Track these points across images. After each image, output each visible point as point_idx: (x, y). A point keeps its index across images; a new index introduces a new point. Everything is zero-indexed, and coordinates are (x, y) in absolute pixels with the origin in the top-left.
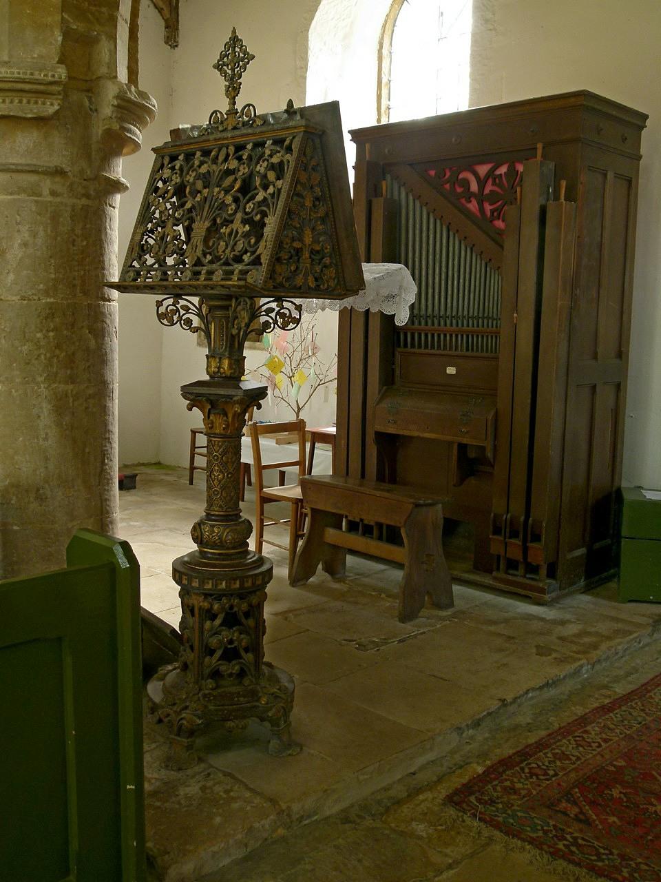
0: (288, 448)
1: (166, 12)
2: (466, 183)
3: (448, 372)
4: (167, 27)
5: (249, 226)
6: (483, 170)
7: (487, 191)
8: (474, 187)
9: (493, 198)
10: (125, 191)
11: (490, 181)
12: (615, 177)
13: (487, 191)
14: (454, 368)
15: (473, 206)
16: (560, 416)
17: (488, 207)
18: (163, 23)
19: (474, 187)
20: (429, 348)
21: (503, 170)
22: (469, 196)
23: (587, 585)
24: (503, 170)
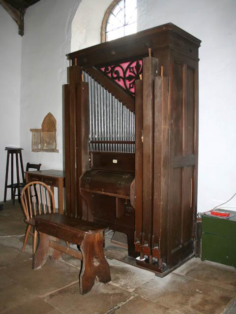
0: (149, 133)
1: (19, 22)
2: (117, 72)
3: (114, 162)
4: (19, 28)
5: (115, 164)
6: (125, 65)
7: (127, 75)
8: (121, 74)
9: (130, 78)
10: (52, 115)
11: (128, 71)
12: (188, 68)
13: (127, 75)
14: (116, 160)
15: (121, 83)
16: (164, 185)
17: (128, 83)
18: (18, 27)
19: (121, 74)
20: (117, 199)
21: (134, 65)
22: (119, 78)
23: (21, 11)
24: (134, 65)
